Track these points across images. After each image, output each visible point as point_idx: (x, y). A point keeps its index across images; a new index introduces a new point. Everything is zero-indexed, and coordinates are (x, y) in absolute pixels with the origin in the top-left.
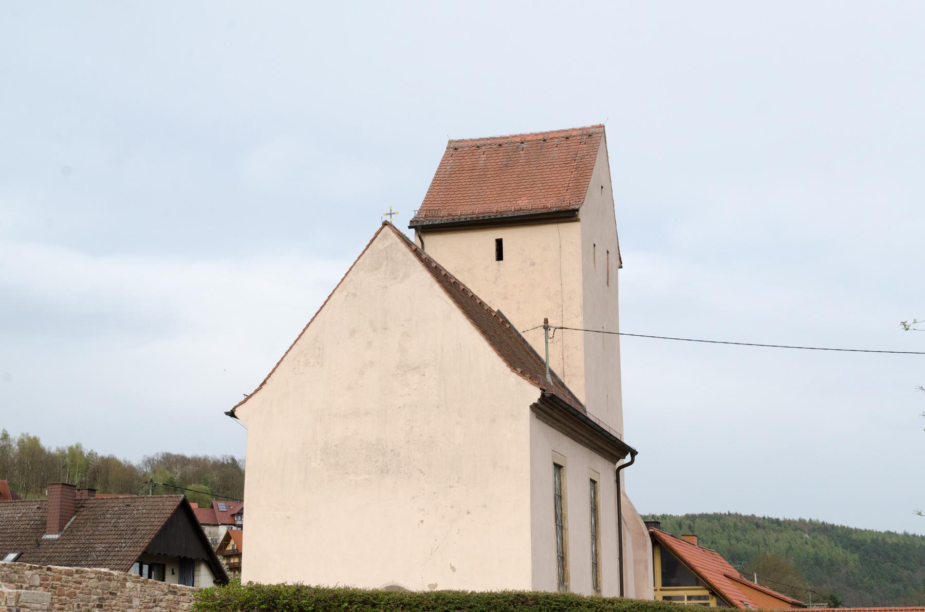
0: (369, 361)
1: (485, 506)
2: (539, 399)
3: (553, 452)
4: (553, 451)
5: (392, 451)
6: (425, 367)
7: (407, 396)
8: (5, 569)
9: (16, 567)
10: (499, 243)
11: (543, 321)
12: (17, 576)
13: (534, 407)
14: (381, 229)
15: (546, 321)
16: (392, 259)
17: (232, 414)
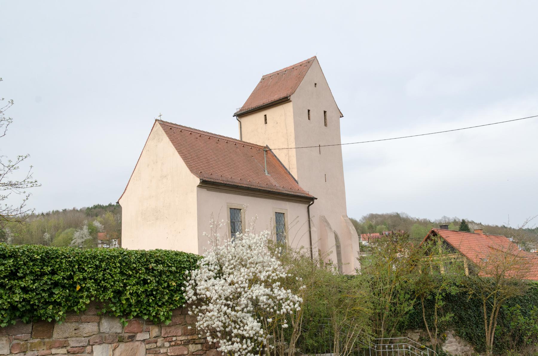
1: (184, 229)
13: (199, 186)
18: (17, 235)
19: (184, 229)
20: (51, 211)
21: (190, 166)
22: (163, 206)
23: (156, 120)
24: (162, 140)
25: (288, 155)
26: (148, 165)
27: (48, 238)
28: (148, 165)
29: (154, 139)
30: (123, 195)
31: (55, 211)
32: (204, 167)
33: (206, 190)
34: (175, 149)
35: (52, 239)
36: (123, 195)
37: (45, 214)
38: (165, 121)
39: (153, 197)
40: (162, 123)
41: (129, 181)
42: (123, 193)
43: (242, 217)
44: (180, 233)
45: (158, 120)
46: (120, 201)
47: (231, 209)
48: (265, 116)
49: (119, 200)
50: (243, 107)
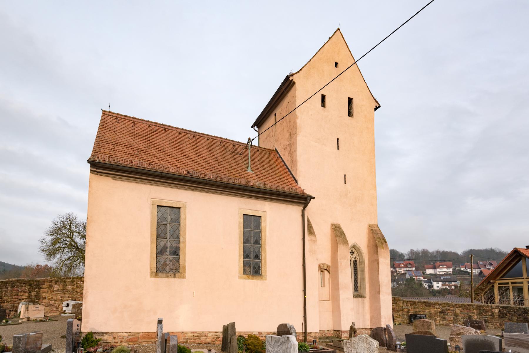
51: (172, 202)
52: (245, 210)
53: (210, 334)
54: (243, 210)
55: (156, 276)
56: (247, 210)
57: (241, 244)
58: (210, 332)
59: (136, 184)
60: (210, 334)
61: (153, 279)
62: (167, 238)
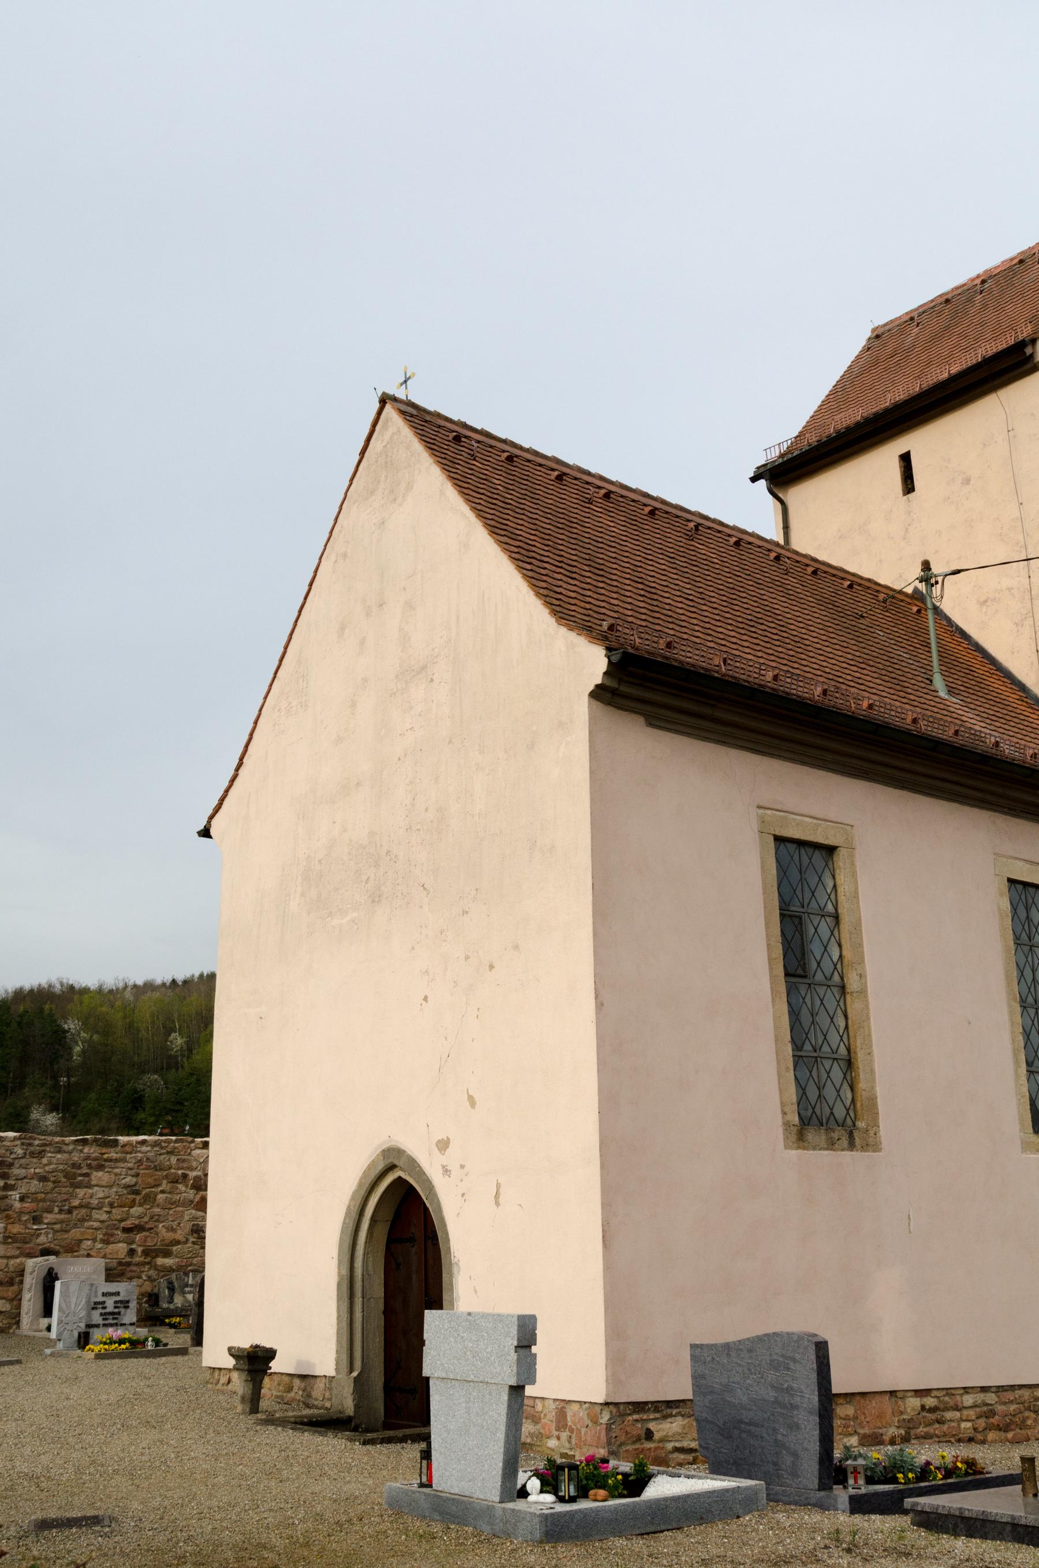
0: (362, 679)
1: (516, 947)
2: (605, 673)
3: (761, 811)
4: (759, 807)
5: (388, 852)
6: (434, 663)
7: (409, 731)
8: (144, 1148)
9: (172, 1144)
10: (906, 459)
11: (920, 567)
12: (174, 1160)
13: (599, 694)
14: (379, 413)
15: (926, 566)
16: (392, 464)
17: (205, 833)
18: (95, 1037)
19: (516, 947)
20: (197, 975)
21: (551, 594)
22: (409, 829)
23: (384, 400)
24: (409, 487)
25: (1030, 621)
26: (342, 628)
27: (179, 1048)
28: (342, 628)
29: (372, 492)
30: (227, 791)
31: (205, 975)
32: (630, 613)
33: (641, 720)
34: (471, 516)
35: (190, 1050)
36: (227, 791)
37: (180, 983)
38: (431, 408)
39: (358, 784)
40: (403, 407)
41: (256, 722)
42: (226, 784)
43: (840, 890)
44: (491, 967)
45: (395, 399)
46: (214, 822)
47: (779, 840)
48: (906, 459)
49: (211, 817)
50: (801, 434)
51: (815, 824)
52: (1009, 860)
53: (968, 1400)
54: (1004, 859)
55: (801, 1144)
56: (1014, 861)
57: (1013, 1003)
58: (966, 1390)
59: (745, 752)
60: (968, 1400)
61: (794, 1153)
62: (805, 977)
